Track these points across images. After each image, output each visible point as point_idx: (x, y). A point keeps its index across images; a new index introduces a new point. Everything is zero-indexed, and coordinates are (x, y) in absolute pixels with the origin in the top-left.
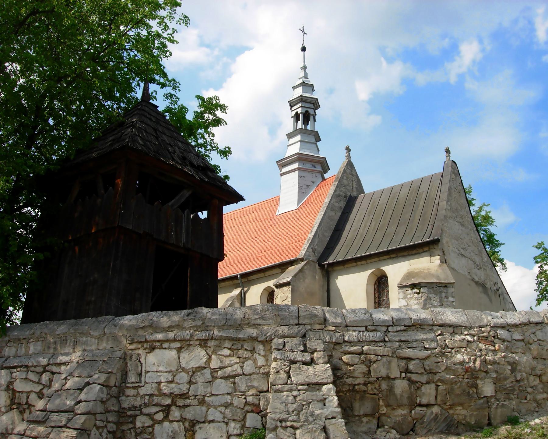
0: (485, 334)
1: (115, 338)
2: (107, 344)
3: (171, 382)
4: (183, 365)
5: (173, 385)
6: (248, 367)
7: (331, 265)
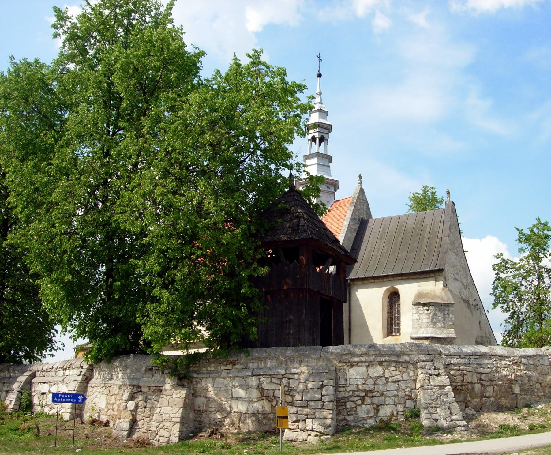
0: (516, 361)
1: (328, 360)
2: (323, 362)
3: (364, 384)
4: (370, 375)
5: (365, 386)
6: (405, 376)
7: (352, 280)
